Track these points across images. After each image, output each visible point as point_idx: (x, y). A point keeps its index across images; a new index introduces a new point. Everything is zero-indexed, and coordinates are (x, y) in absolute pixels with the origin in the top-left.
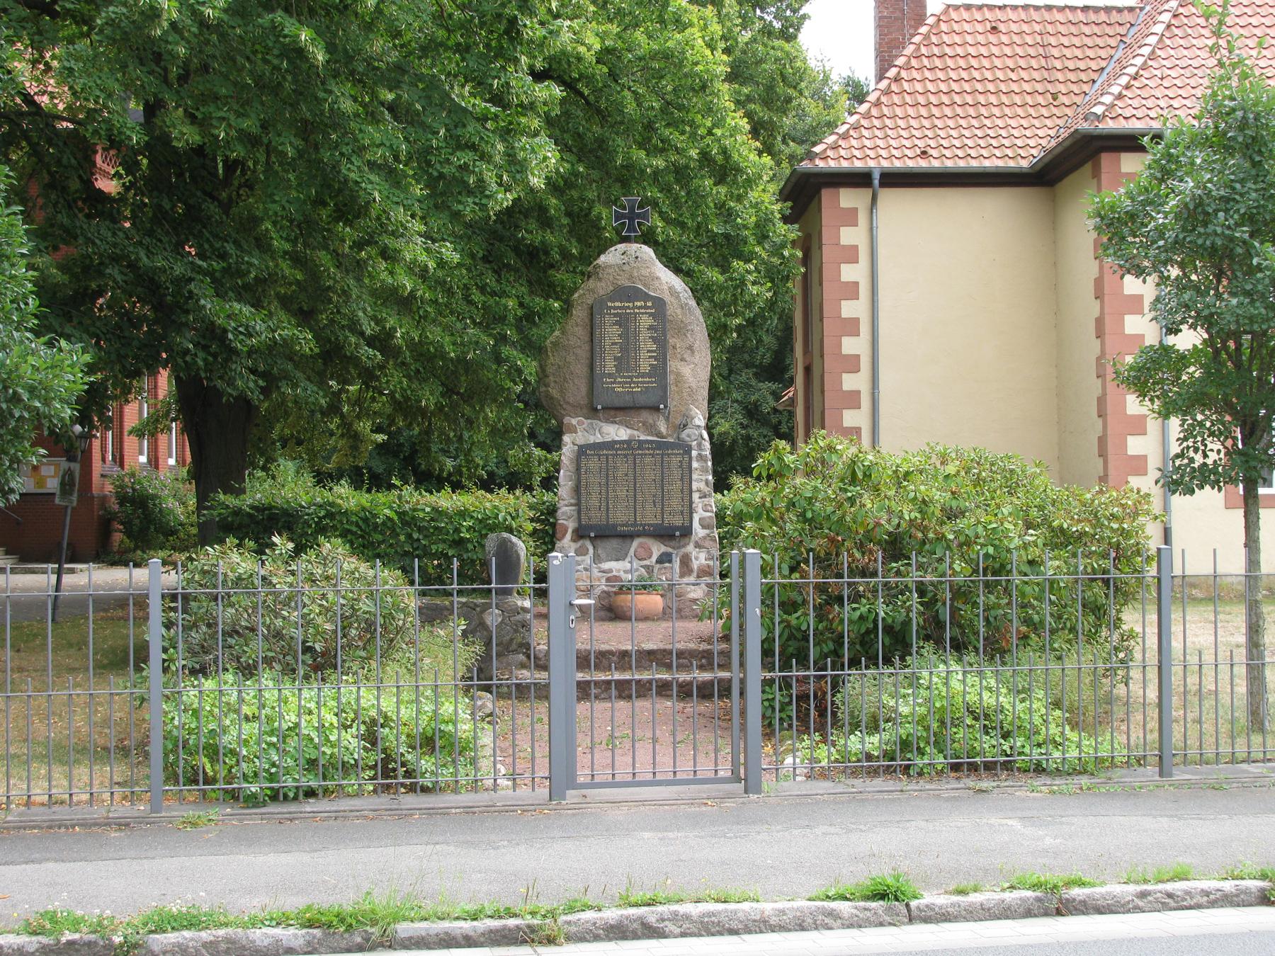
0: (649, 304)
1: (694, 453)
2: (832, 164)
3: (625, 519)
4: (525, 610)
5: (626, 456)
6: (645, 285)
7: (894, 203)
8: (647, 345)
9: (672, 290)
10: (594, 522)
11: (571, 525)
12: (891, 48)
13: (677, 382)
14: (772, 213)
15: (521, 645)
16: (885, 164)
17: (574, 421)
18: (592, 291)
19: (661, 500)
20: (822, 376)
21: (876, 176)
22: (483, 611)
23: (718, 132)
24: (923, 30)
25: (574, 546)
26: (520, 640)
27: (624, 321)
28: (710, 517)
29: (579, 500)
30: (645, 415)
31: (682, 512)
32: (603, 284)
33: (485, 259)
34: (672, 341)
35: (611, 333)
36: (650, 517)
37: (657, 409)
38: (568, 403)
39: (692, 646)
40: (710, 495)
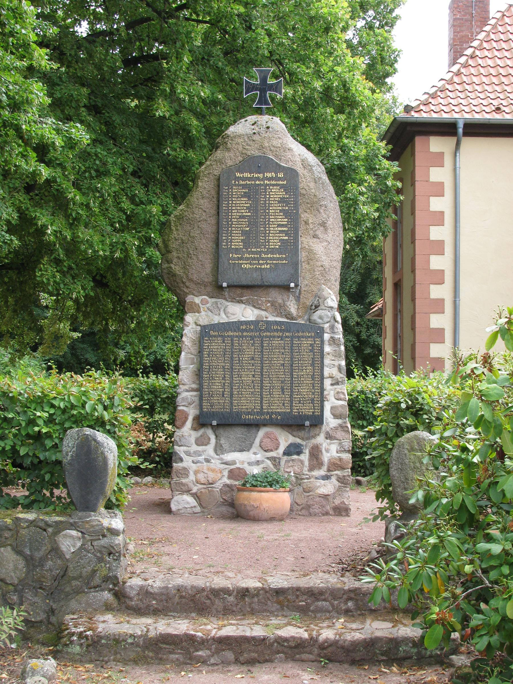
0: (281, 175)
1: (326, 336)
2: (425, 115)
3: (251, 406)
4: (114, 532)
5: (252, 338)
6: (276, 156)
7: (473, 148)
8: (277, 219)
9: (305, 163)
10: (216, 409)
11: (192, 412)
12: (462, 43)
13: (309, 260)
14: (379, 149)
15: (106, 579)
16: (467, 116)
17: (197, 300)
18: (220, 161)
19: (290, 387)
20: (413, 288)
21: (461, 126)
22: (57, 533)
23: (339, 69)
24: (487, 28)
25: (194, 435)
26: (104, 572)
27: (253, 193)
28: (342, 406)
29: (201, 385)
30: (276, 296)
31: (313, 400)
32: (232, 154)
33: (134, 174)
34: (304, 216)
35: (239, 206)
36: (277, 405)
37: (287, 288)
38: (191, 280)
39: (333, 580)
40: (343, 382)
